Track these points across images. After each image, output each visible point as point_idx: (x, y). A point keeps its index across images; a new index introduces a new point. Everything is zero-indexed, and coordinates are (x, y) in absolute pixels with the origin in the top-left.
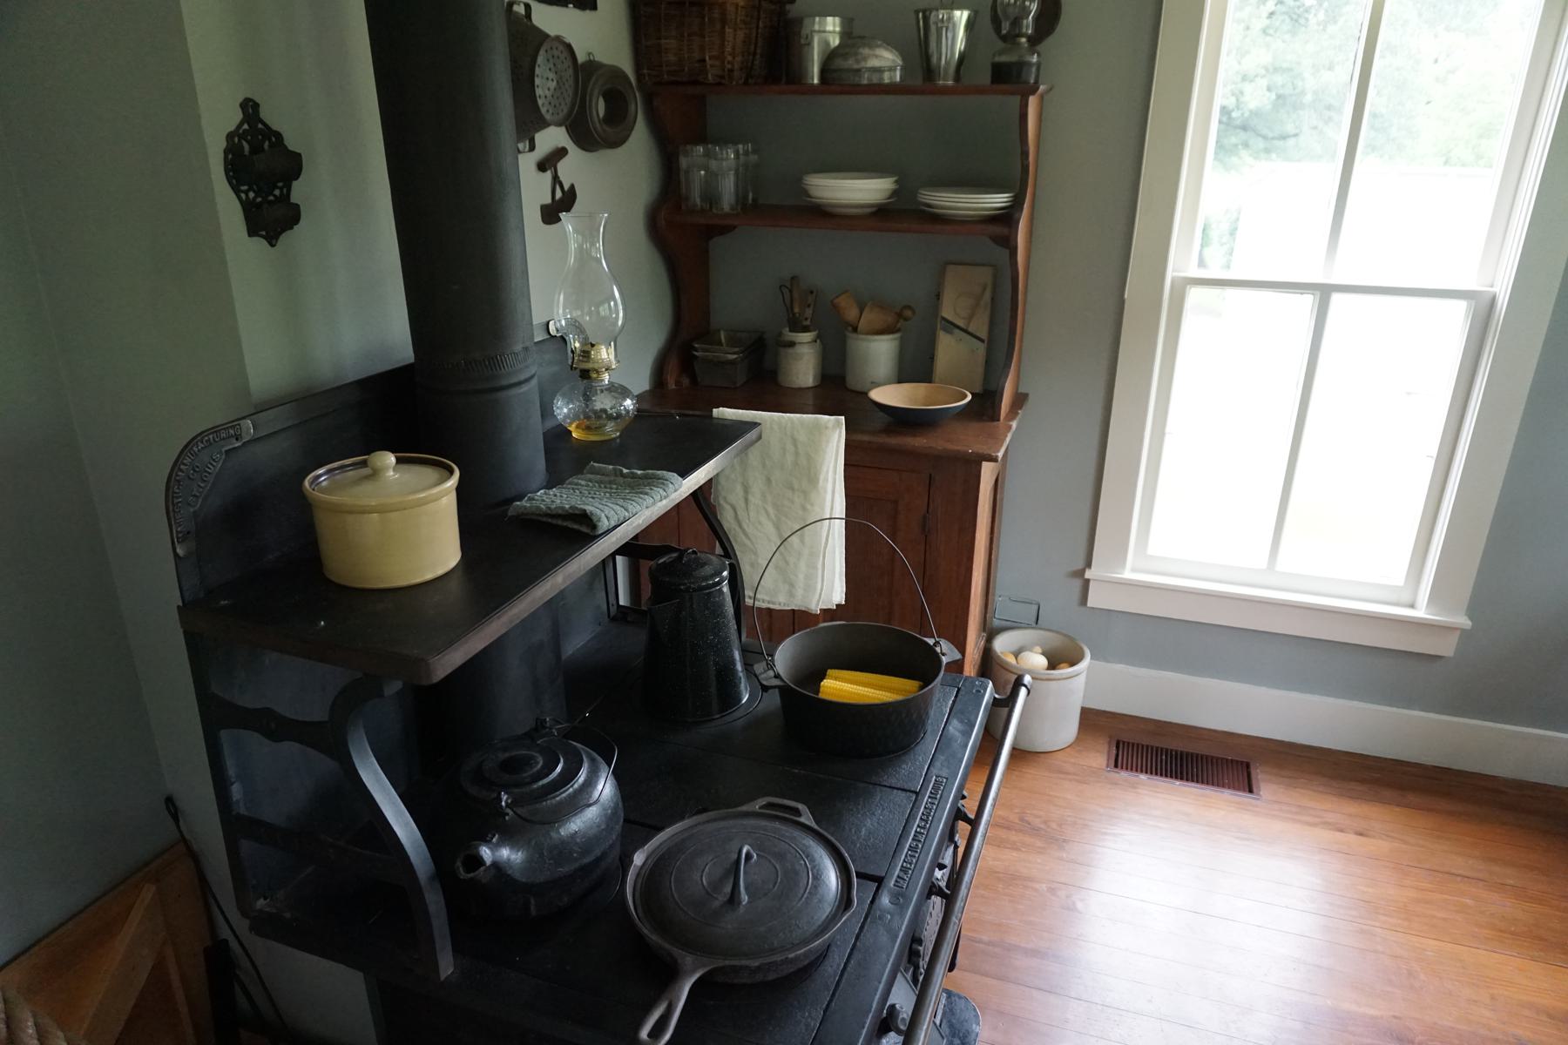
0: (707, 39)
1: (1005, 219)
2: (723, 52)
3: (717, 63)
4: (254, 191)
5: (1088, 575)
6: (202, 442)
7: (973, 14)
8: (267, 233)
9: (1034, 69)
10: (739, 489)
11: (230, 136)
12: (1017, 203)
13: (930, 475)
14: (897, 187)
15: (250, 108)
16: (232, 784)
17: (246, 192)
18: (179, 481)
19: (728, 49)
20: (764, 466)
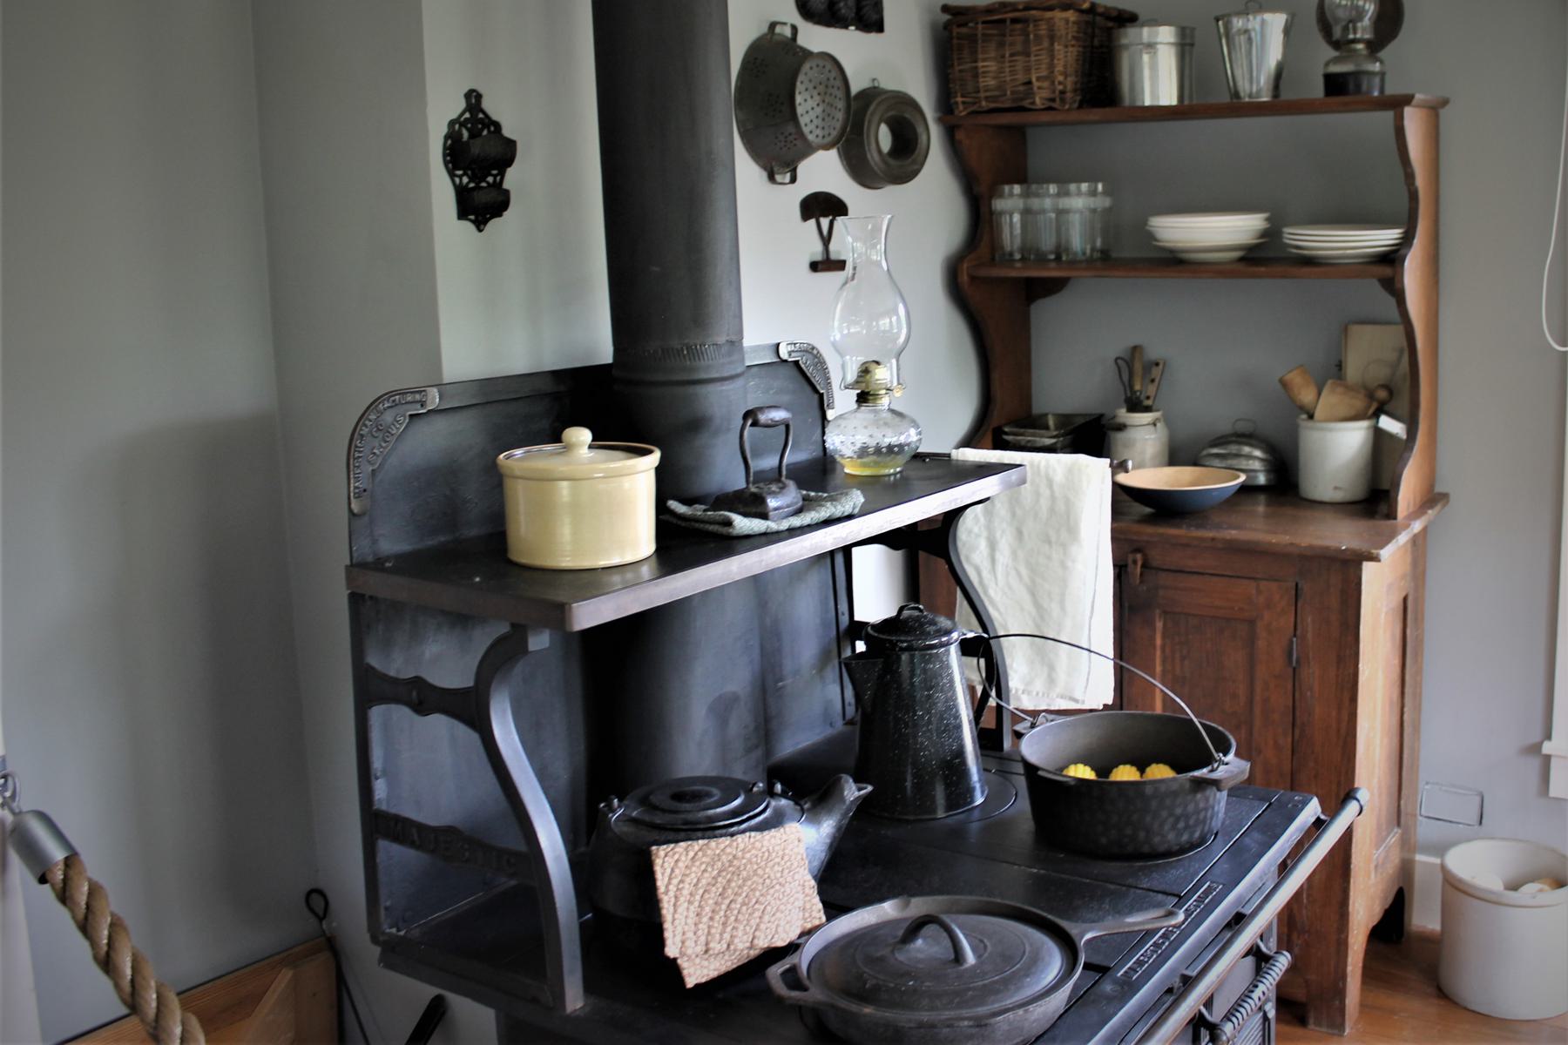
0: (1033, 58)
1: (1390, 259)
2: (1053, 72)
3: (1046, 84)
4: (469, 177)
5: (1547, 748)
6: (388, 401)
7: (1290, 19)
8: (476, 217)
9: (1377, 80)
10: (983, 545)
11: (452, 123)
12: (1407, 240)
13: (1297, 585)
14: (1268, 226)
15: (474, 99)
16: (377, 778)
17: (460, 177)
18: (362, 436)
19: (1059, 68)
20: (1014, 514)
